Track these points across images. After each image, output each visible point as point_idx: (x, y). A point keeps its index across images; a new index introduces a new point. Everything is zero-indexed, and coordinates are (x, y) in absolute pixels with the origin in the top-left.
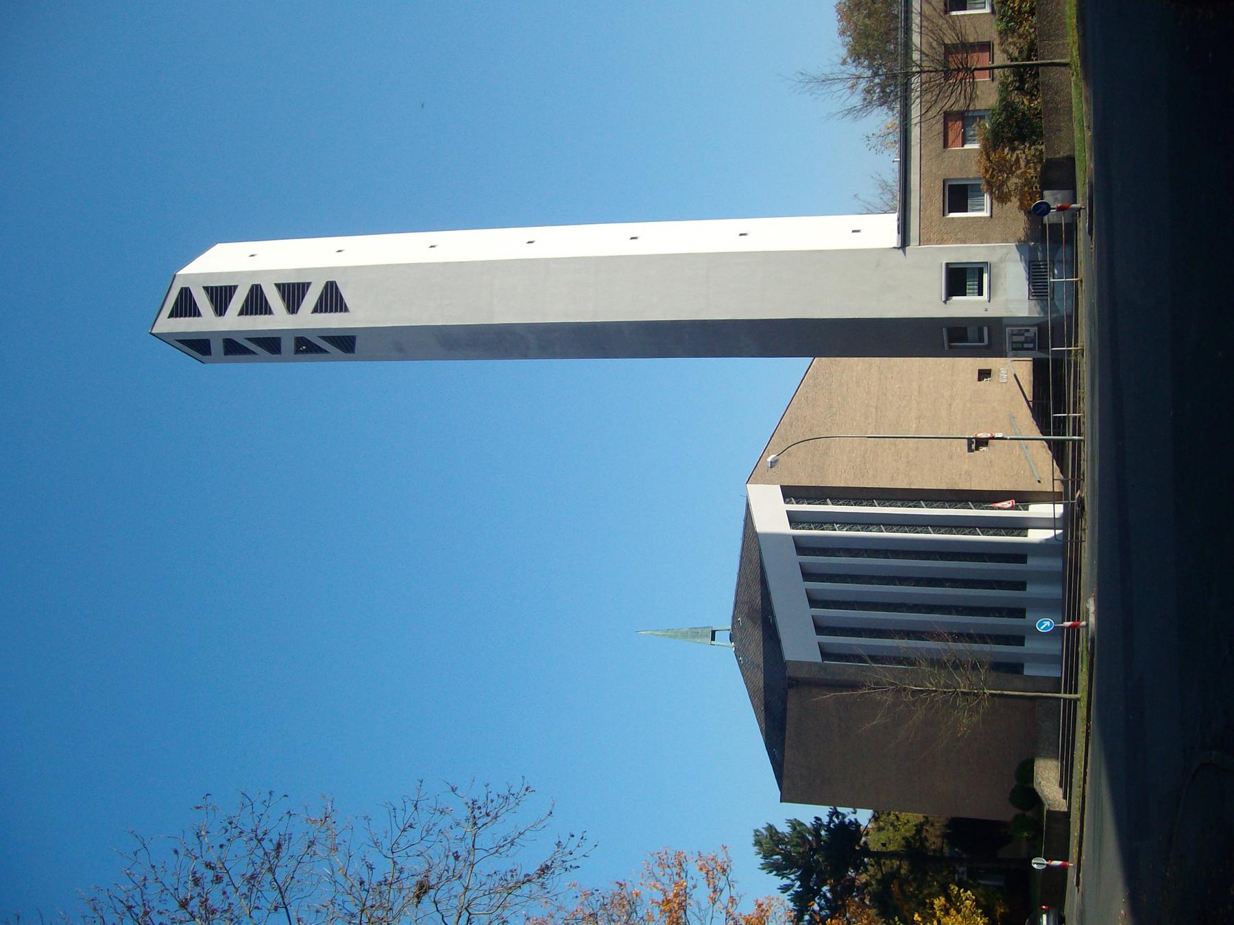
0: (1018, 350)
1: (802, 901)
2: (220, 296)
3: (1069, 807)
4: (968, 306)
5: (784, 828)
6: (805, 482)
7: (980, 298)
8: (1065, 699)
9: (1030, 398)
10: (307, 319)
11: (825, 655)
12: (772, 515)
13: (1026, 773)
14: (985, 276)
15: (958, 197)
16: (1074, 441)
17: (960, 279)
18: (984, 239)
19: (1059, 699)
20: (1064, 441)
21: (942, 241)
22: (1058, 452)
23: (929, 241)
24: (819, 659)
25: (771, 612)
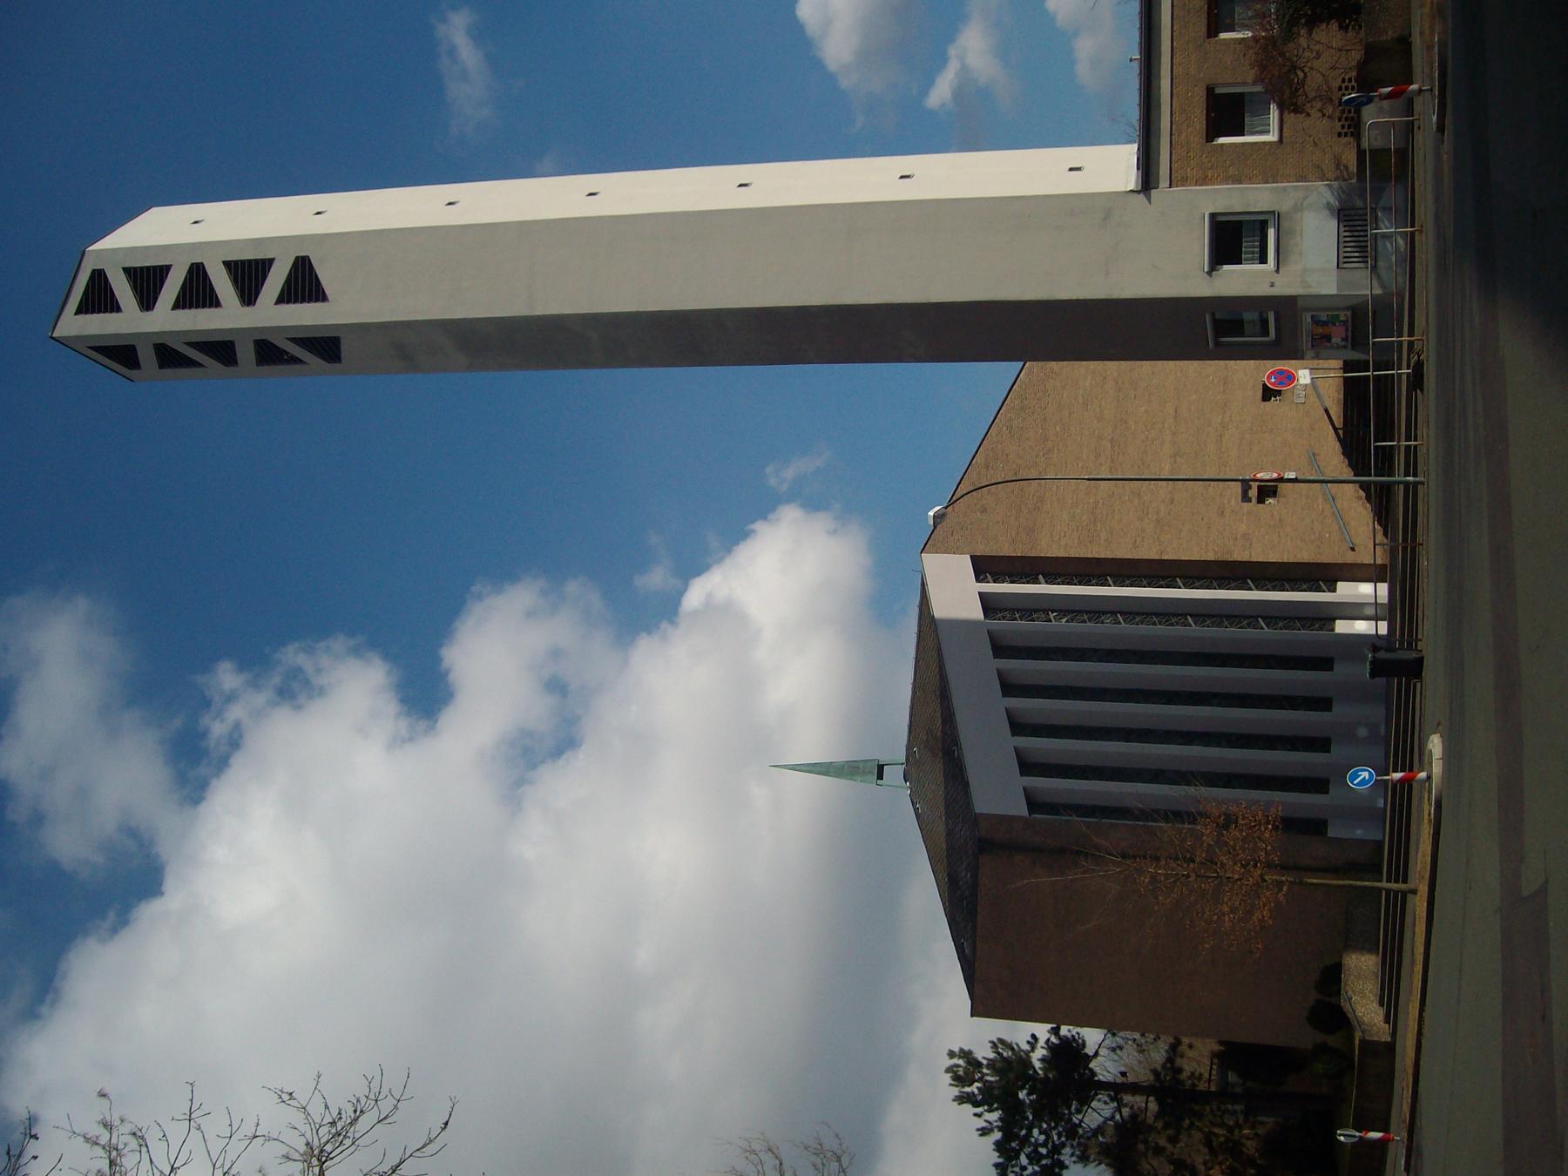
0: (1320, 344)
1: (1007, 1150)
2: (147, 281)
3: (1394, 1034)
4: (1244, 279)
5: (984, 1053)
6: (1006, 551)
7: (1262, 266)
8: (1388, 891)
9: (1339, 423)
10: (270, 313)
11: (1034, 803)
12: (956, 592)
13: (1332, 977)
14: (1271, 233)
15: (1226, 113)
16: (1407, 484)
17: (1231, 239)
18: (1269, 176)
19: (1380, 890)
20: (1389, 486)
21: (1204, 181)
22: (1381, 502)
23: (1184, 181)
24: (1023, 810)
25: (955, 741)
